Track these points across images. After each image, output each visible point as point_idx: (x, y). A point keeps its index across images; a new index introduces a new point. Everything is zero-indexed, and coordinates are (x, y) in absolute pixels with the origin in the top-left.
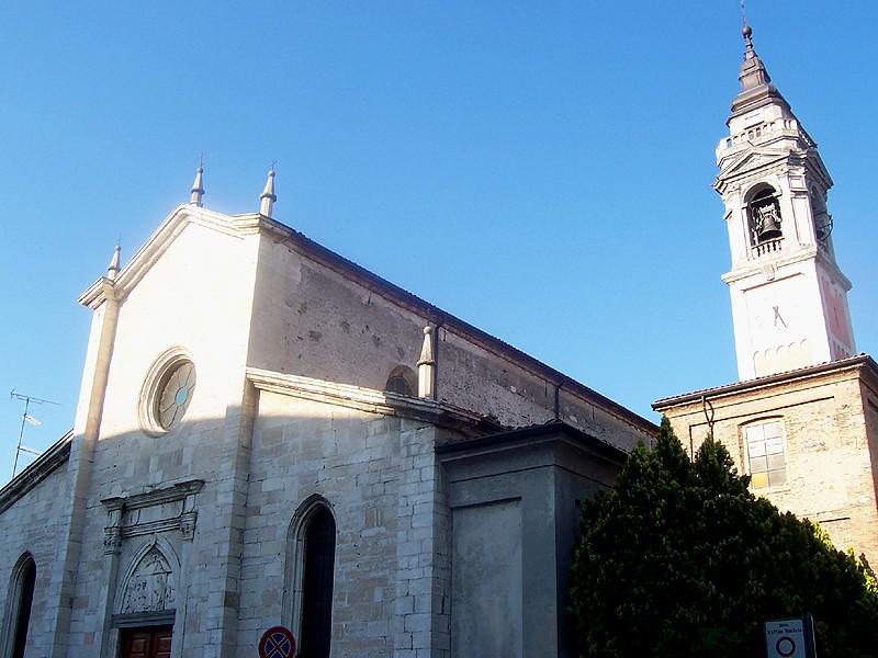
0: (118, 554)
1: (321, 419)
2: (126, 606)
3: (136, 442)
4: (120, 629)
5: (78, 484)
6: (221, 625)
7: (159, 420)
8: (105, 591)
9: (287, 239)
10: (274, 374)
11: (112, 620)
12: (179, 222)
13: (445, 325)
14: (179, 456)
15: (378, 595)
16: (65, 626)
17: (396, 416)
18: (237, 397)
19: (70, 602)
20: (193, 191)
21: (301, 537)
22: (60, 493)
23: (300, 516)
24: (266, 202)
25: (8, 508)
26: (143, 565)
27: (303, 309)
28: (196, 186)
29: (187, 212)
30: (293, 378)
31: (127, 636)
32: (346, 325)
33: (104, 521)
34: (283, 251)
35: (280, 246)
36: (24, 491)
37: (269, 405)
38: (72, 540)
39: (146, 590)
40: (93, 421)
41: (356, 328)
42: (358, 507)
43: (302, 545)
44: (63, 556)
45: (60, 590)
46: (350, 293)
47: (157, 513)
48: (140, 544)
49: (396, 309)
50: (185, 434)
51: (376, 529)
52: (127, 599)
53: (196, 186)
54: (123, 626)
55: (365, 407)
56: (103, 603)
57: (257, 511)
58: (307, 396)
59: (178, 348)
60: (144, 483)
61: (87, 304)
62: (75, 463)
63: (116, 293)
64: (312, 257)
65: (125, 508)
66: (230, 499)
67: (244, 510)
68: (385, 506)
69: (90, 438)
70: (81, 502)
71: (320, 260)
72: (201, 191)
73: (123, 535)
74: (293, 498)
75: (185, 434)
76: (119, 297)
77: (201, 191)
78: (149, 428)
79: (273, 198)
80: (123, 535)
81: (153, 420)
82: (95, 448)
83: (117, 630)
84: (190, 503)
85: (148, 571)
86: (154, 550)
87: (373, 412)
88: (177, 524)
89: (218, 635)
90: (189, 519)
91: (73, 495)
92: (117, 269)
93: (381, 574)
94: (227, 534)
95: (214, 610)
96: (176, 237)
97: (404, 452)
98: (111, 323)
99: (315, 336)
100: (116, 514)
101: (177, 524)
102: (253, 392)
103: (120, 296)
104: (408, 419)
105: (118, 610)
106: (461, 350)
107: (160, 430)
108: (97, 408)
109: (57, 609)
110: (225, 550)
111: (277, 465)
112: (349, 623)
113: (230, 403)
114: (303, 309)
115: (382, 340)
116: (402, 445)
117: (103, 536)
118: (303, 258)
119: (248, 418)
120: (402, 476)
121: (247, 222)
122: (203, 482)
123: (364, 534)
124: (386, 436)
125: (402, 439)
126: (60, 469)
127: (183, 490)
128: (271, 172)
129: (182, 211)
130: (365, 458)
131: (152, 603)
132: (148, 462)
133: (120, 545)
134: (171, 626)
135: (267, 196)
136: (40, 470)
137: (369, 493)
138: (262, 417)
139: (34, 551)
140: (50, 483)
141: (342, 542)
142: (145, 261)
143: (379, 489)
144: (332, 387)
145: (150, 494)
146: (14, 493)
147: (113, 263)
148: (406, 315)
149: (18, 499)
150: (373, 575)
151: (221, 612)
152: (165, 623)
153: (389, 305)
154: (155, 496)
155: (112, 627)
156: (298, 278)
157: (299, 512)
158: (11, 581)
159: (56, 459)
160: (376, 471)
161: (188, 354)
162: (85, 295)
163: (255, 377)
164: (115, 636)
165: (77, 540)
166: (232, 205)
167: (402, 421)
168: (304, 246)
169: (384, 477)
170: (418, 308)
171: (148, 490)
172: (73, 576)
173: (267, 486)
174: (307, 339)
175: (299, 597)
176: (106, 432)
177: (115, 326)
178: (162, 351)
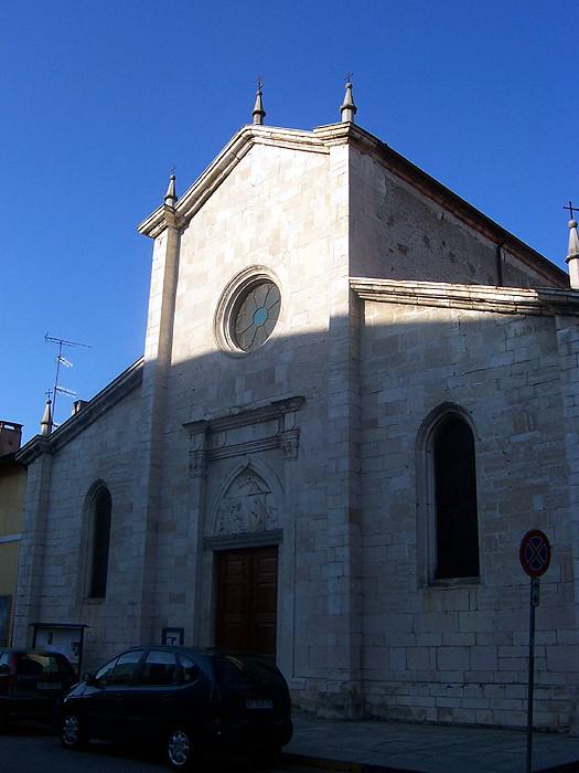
0: (205, 477)
1: (446, 324)
2: (219, 527)
3: (216, 364)
4: (215, 552)
5: (154, 407)
6: (347, 541)
7: (236, 339)
8: (195, 515)
9: (376, 151)
10: (386, 282)
11: (205, 543)
12: (243, 144)
13: (505, 246)
14: (270, 374)
15: (538, 503)
16: (153, 551)
17: (541, 315)
18: (343, 307)
19: (155, 526)
20: (256, 112)
21: (430, 448)
22: (132, 425)
23: (428, 426)
24: (346, 115)
25: (74, 438)
26: (235, 486)
27: (391, 222)
28: (257, 108)
29: (254, 132)
30: (413, 284)
31: (222, 557)
32: (426, 240)
33: (186, 447)
34: (369, 162)
35: (365, 157)
36: (91, 421)
37: (374, 314)
38: (152, 465)
39: (241, 512)
40: (165, 348)
41: (435, 243)
42: (503, 412)
43: (430, 456)
44: (145, 481)
45: (145, 515)
46: (428, 209)
47: (247, 434)
48: (230, 466)
49: (465, 227)
50: (276, 352)
51: (529, 434)
52: (218, 522)
53: (257, 107)
54: (217, 549)
55: (502, 308)
56: (194, 527)
57: (374, 424)
58: (431, 301)
59: (256, 268)
60: (230, 404)
61: (147, 233)
62: (148, 390)
63: (177, 220)
64: (394, 170)
65: (209, 429)
66: (346, 413)
67: (361, 423)
68: (538, 409)
69: (162, 364)
70: (159, 429)
71: (401, 174)
72: (262, 113)
73: (210, 458)
74: (419, 406)
75: (276, 352)
76: (180, 225)
77: (262, 113)
78: (229, 349)
79: (353, 109)
80: (210, 458)
81: (230, 341)
82: (166, 370)
83: (212, 553)
84: (290, 421)
85: (242, 492)
86: (247, 471)
87: (512, 313)
88: (276, 443)
89: (345, 553)
90: (291, 437)
91: (150, 420)
92: (175, 198)
93: (540, 480)
94: (345, 447)
95: (336, 526)
96: (239, 160)
97: (563, 350)
98: (174, 250)
99: (403, 250)
100: (200, 439)
101: (276, 443)
102: (358, 300)
103: (181, 224)
104: (564, 315)
105: (210, 533)
106: (517, 270)
107: (239, 350)
108: (166, 335)
109: (144, 535)
110: (345, 464)
111: (395, 377)
112: (503, 533)
113: (333, 313)
114: (391, 222)
115: (457, 257)
116: (559, 343)
117: (187, 460)
118: (386, 171)
119: (352, 326)
120: (563, 376)
121: (334, 132)
122: (303, 399)
123: (514, 439)
124: (530, 337)
125: (559, 338)
126: (129, 398)
127: (279, 409)
128: (348, 84)
129: (248, 132)
130: (505, 360)
131: (249, 524)
132: (234, 382)
133: (206, 468)
134: (277, 546)
135: (348, 107)
136: (107, 399)
137: (516, 397)
138: (370, 327)
139: (106, 478)
140: (119, 411)
141: (486, 449)
142: (207, 186)
143: (527, 392)
144: (462, 291)
145: (239, 414)
146: (79, 423)
147: (170, 192)
148: (473, 233)
149: (84, 429)
150: (530, 481)
151: (346, 528)
152: (272, 543)
153: (458, 222)
154: (245, 417)
155: (205, 550)
156: (384, 191)
157: (426, 422)
158: (85, 510)
159: (128, 386)
160: (522, 374)
161: (271, 274)
162: (146, 224)
163: (357, 287)
164: (209, 558)
165: (158, 466)
166: (303, 117)
167: (557, 318)
168: (391, 159)
169: (533, 379)
170: (483, 226)
171: (236, 411)
172: (157, 502)
173: (385, 397)
174: (397, 252)
175: (432, 510)
176: (178, 355)
177: (178, 253)
178: (238, 271)
